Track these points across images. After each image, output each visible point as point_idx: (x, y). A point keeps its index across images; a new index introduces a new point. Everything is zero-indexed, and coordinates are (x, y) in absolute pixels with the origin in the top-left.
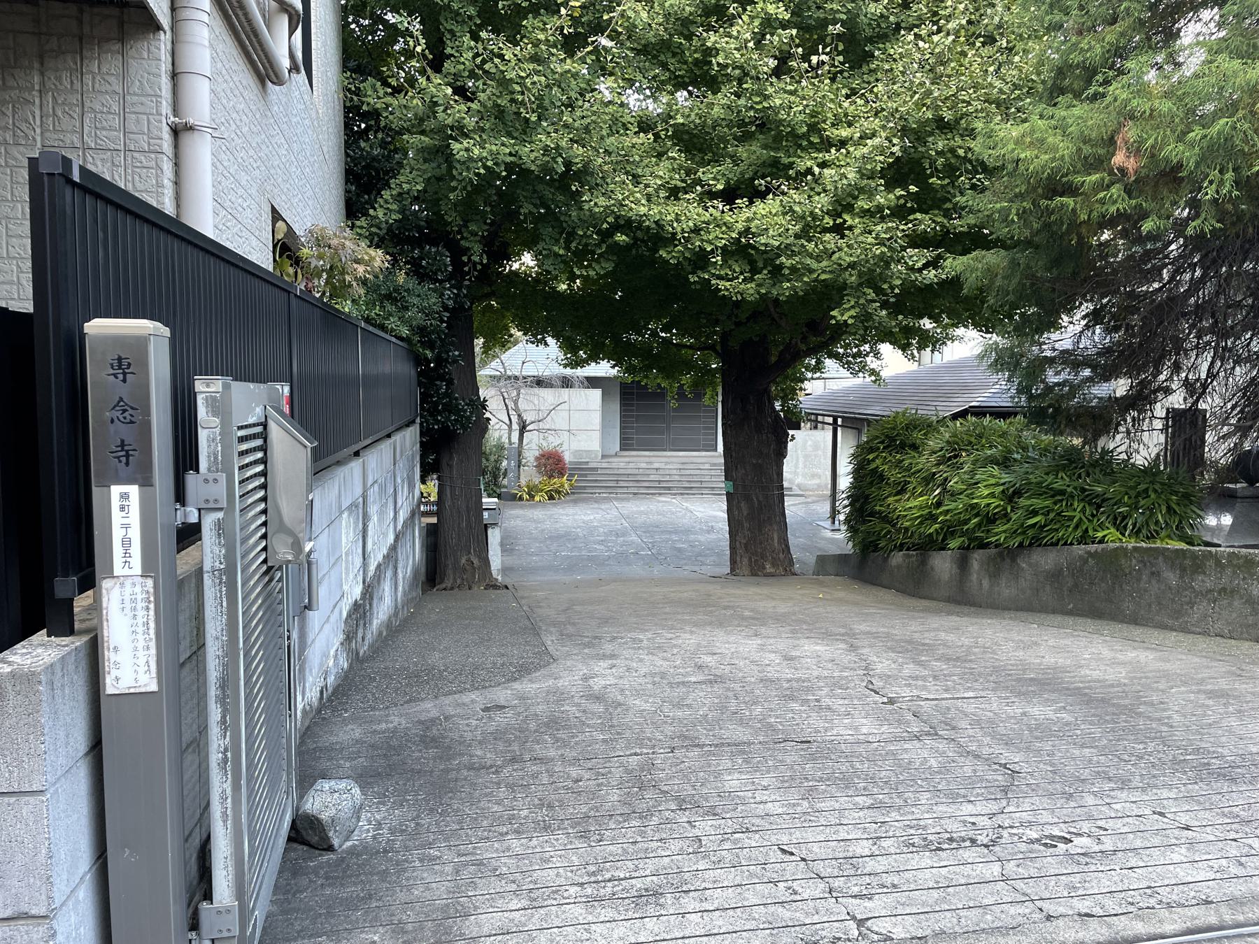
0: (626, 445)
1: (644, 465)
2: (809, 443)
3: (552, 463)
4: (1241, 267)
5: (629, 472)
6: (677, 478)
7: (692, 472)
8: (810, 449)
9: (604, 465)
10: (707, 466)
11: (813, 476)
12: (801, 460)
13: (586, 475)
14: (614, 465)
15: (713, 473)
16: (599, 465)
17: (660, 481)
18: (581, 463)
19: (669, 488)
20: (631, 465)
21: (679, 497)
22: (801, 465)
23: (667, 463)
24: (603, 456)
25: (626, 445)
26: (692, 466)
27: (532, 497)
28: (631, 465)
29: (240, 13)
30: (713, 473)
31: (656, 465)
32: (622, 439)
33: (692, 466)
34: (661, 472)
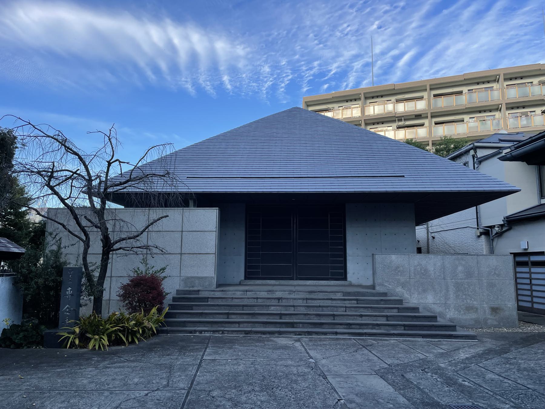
0: (251, 274)
1: (264, 294)
2: (460, 268)
3: (145, 290)
4: (14, 230)
5: (245, 302)
6: (303, 310)
7: (322, 303)
8: (461, 275)
9: (218, 294)
10: (339, 296)
11: (469, 309)
12: (452, 289)
13: (191, 307)
14: (229, 295)
15: (347, 304)
16: (211, 295)
17: (281, 315)
18: (190, 292)
19: (292, 325)
20: (249, 294)
21: (305, 339)
22: (452, 295)
23: (291, 292)
24: (219, 285)
25: (251, 274)
26: (321, 296)
27: (84, 340)
28: (249, 294)
29: (467, 98)
30: (347, 304)
31: (278, 294)
32: (247, 267)
33: (321, 296)
34: (284, 303)
